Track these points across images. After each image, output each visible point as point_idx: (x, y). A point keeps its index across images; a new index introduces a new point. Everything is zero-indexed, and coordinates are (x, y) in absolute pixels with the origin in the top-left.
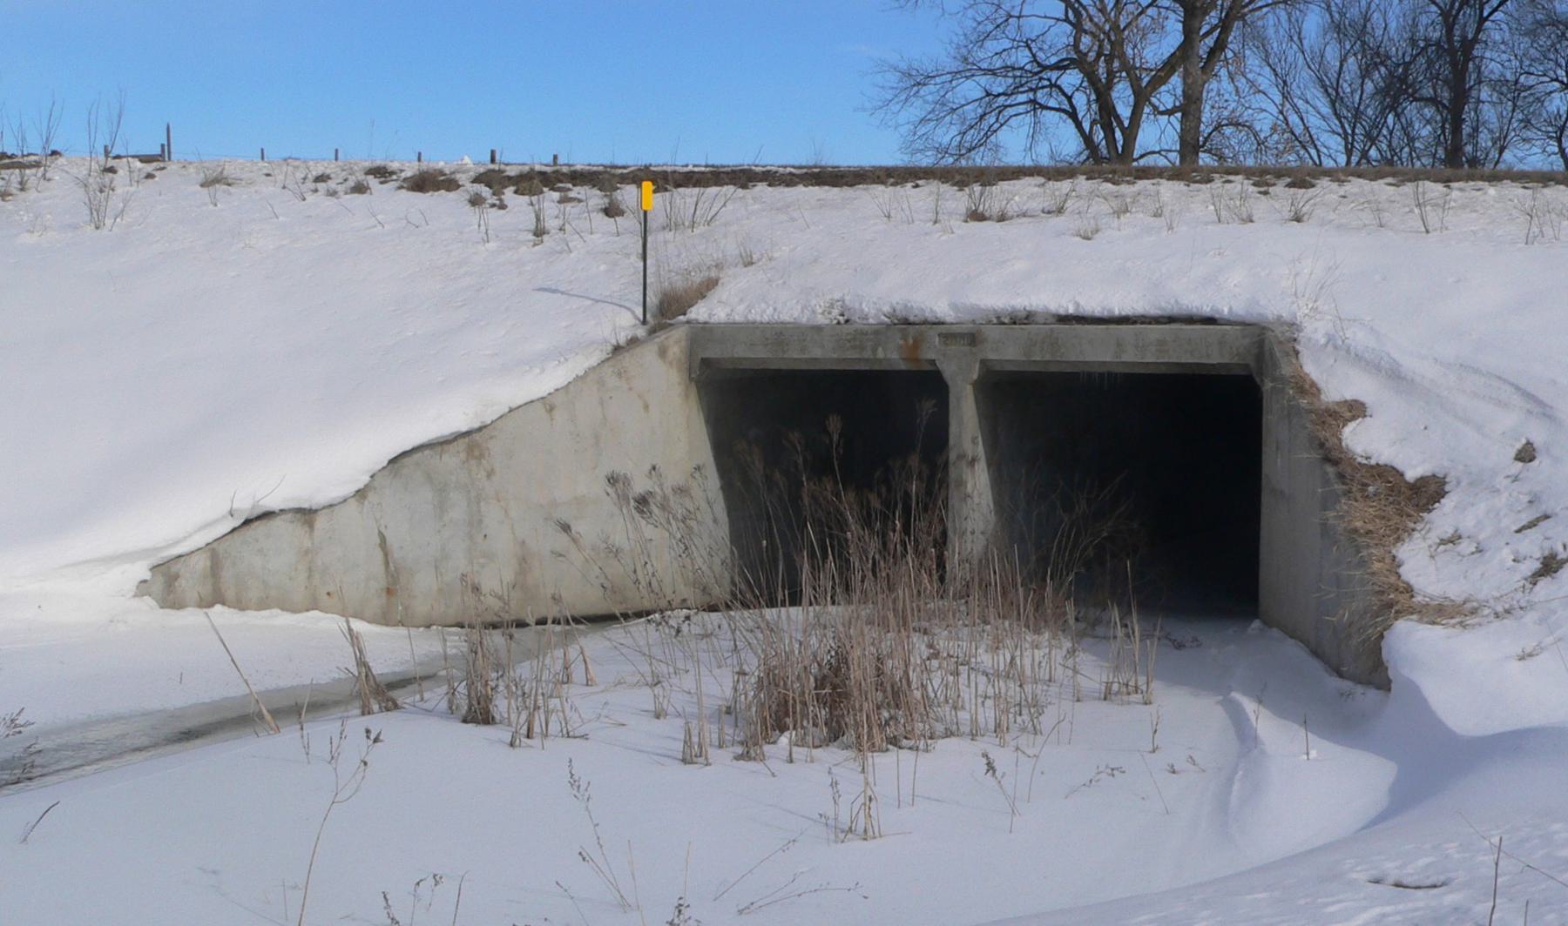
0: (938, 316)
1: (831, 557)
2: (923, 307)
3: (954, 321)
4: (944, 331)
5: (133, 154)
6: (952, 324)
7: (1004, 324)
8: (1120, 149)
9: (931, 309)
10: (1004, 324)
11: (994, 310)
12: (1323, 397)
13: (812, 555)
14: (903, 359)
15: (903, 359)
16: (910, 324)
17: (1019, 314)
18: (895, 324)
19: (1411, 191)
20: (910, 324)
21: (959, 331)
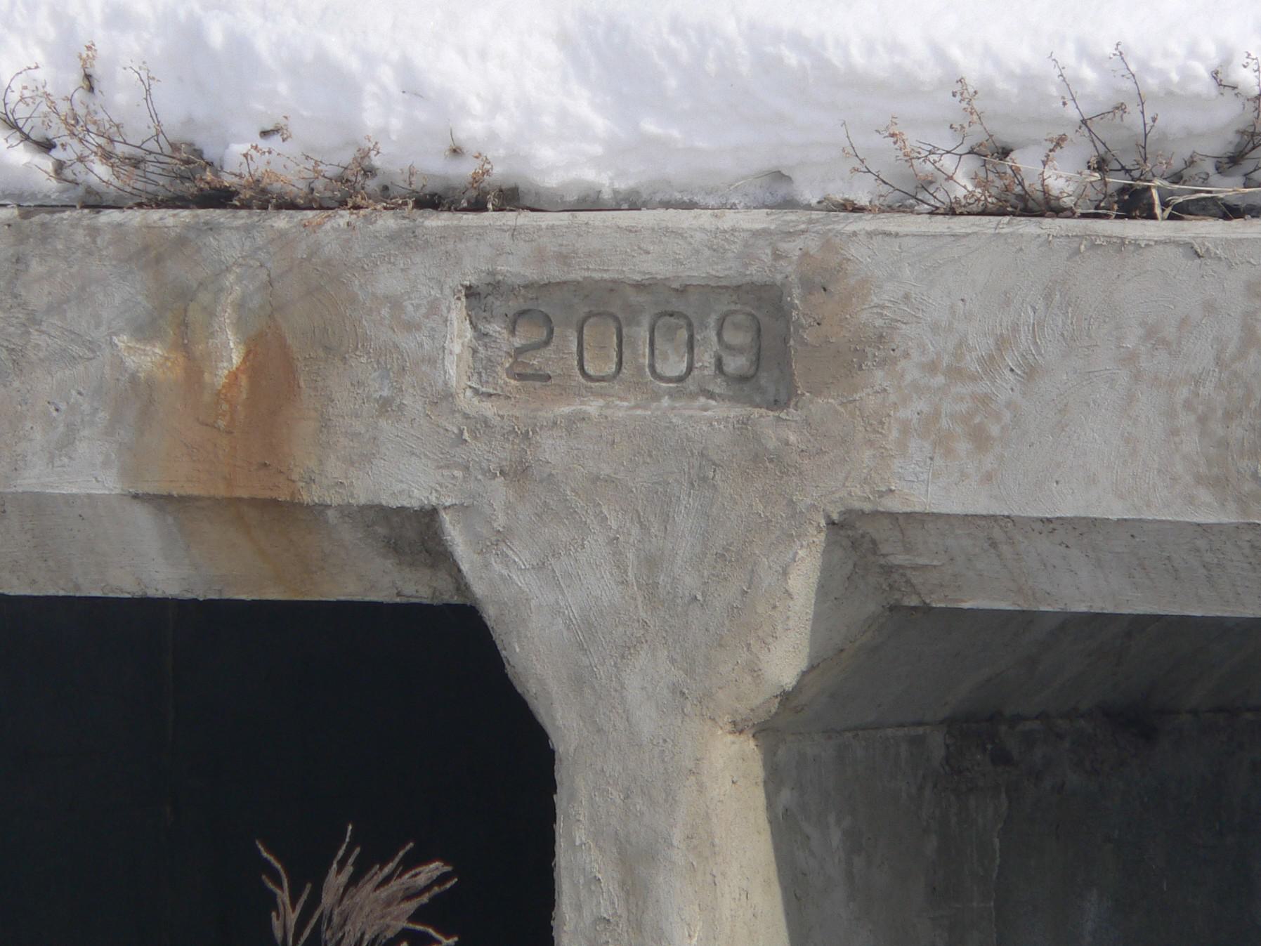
0: (471, 129)
1: (367, 937)
2: (336, 47)
3: (604, 180)
4: (515, 267)
5: (74, 89)
6: (590, 202)
7: (1048, 207)
8: (309, 886)
9: (406, 69)
10: (1048, 207)
11: (960, 89)
12: (521, 202)
13: (330, 920)
14: (161, 502)
15: (161, 502)
16: (220, 198)
17: (1173, 121)
18: (95, 202)
19: (960, 193)
20: (220, 198)
21: (652, 266)
